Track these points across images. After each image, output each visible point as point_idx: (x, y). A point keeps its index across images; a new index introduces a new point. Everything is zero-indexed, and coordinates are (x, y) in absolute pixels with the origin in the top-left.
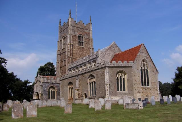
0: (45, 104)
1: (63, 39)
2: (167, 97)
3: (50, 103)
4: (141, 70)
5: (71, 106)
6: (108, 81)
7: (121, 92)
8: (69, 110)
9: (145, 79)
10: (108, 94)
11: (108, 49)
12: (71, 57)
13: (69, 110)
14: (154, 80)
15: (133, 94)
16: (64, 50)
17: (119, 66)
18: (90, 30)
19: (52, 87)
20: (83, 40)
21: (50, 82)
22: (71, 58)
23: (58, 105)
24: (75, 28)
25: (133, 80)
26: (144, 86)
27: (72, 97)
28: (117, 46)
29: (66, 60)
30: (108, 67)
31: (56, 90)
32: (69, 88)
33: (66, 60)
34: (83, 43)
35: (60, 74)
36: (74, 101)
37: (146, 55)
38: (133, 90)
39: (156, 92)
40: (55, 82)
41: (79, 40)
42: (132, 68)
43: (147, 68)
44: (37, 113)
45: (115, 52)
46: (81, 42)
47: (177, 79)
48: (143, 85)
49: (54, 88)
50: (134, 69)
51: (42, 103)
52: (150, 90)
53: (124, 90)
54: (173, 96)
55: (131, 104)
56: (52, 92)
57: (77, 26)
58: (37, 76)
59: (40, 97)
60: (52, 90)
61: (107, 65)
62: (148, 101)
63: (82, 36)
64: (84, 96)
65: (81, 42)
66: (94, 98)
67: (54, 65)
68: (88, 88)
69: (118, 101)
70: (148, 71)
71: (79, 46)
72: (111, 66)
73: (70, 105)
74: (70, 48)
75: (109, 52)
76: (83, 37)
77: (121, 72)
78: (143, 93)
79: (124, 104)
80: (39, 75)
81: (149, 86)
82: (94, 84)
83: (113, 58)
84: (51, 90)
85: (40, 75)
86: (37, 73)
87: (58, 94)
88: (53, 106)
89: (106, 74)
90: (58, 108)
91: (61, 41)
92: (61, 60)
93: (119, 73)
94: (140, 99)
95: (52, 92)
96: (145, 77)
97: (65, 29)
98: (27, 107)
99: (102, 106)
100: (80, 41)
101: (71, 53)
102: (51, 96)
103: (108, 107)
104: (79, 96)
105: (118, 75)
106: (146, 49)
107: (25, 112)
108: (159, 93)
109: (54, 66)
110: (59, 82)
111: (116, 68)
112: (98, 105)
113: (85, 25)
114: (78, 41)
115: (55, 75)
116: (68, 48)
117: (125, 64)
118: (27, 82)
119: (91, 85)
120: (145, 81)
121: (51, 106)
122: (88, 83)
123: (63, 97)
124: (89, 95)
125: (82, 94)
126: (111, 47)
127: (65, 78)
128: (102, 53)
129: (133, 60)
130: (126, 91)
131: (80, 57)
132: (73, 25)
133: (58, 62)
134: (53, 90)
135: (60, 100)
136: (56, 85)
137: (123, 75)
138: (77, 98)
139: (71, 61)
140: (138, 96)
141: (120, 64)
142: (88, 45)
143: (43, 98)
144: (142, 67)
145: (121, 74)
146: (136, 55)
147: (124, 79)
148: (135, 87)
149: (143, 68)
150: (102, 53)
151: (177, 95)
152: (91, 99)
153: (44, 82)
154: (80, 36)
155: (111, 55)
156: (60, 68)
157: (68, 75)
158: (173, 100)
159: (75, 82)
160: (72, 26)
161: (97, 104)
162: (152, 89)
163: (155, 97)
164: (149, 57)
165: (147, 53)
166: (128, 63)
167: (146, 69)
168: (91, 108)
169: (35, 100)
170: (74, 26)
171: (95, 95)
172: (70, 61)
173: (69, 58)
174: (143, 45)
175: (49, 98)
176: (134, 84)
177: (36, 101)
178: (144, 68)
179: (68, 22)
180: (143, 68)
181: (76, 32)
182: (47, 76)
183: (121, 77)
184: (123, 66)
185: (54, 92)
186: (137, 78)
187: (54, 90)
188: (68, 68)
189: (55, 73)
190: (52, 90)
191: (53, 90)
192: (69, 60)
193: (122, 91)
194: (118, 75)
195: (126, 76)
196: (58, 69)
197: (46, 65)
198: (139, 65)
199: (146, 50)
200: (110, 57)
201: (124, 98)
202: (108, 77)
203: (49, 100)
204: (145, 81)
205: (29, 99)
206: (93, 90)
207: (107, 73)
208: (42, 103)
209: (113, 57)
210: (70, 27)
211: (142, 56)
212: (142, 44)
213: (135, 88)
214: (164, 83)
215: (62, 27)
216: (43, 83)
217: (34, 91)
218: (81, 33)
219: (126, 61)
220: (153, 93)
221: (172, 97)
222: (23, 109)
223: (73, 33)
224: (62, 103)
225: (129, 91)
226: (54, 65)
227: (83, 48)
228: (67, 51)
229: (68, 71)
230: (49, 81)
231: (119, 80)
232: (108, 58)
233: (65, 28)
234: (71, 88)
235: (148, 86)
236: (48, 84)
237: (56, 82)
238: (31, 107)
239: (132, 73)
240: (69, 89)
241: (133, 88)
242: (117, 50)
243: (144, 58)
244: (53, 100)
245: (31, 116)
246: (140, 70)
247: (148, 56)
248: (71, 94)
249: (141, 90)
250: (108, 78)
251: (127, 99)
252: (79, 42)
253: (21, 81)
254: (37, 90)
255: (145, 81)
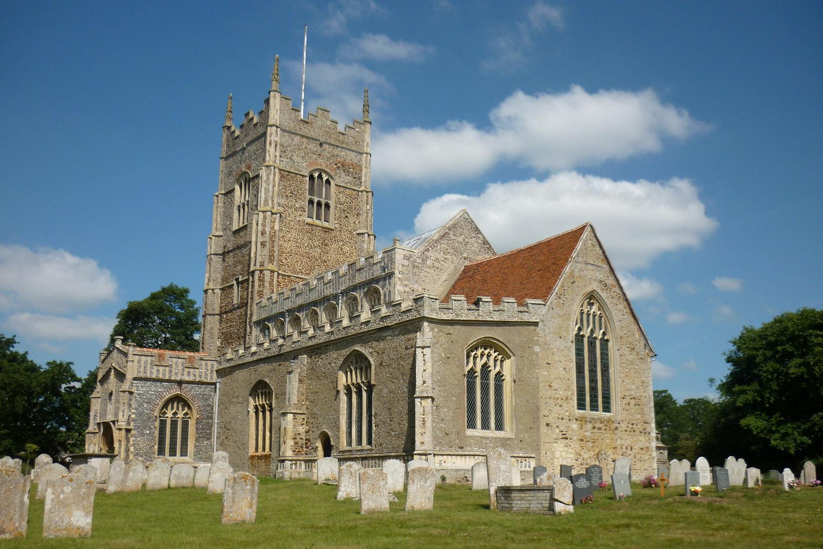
0: (140, 475)
1: (237, 187)
2: (686, 463)
3: (162, 473)
4: (579, 338)
5: (252, 491)
6: (429, 382)
7: (486, 433)
8: (242, 506)
9: (593, 380)
10: (423, 439)
11: (437, 241)
12: (270, 267)
13: (242, 506)
14: (633, 387)
15: (537, 449)
16: (242, 234)
17: (480, 319)
18: (363, 154)
19: (177, 399)
20: (328, 196)
21: (154, 376)
22: (272, 272)
23: (197, 482)
24: (297, 139)
25: (541, 385)
26: (588, 413)
27: (264, 449)
28: (477, 230)
29: (247, 280)
30: (431, 321)
31: (195, 415)
32: (256, 407)
33: (247, 280)
34: (327, 206)
35: (218, 344)
36: (273, 467)
37: (600, 276)
38: (538, 427)
39: (642, 441)
40: (191, 378)
41: (311, 192)
42: (538, 329)
43: (604, 334)
44: (93, 518)
45: (465, 255)
46: (319, 204)
47: (737, 388)
48: (585, 409)
49: (186, 404)
50: (545, 332)
51: (126, 473)
52: (616, 428)
53: (499, 426)
54: (717, 461)
55: (521, 490)
56: (174, 423)
57: (305, 130)
58: (113, 341)
59: (116, 445)
60: (175, 414)
61: (427, 313)
62: (601, 478)
63: (325, 178)
64: (319, 445)
65: (319, 204)
66: (363, 459)
67: (190, 297)
68: (337, 411)
69: (469, 475)
70: (610, 344)
71: (309, 220)
72: (445, 317)
73: (249, 487)
74: (267, 230)
75: (441, 256)
76: (328, 182)
77: (486, 344)
78: (582, 440)
79: (492, 491)
80: (118, 344)
81: (609, 412)
82: (364, 394)
83: (458, 280)
84: (169, 414)
85: (124, 342)
86: (110, 331)
87: (204, 433)
88: (176, 488)
89: (419, 351)
90: (196, 495)
91: (230, 192)
92: (224, 279)
93: (476, 349)
94: (565, 471)
95: (174, 423)
96: (593, 371)
97: (249, 144)
98: (50, 491)
99: (397, 494)
100: (316, 200)
101: (272, 251)
102: (169, 441)
103: (421, 498)
104: (296, 443)
105: (475, 358)
106: (601, 247)
107: (37, 505)
108: (654, 444)
109: (193, 303)
110: (209, 380)
111: (464, 328)
112: (374, 489)
113: (341, 128)
114: (308, 197)
115: (193, 346)
116: (260, 228)
117: (509, 309)
118: (62, 371)
119: (354, 396)
120: (594, 390)
121: (166, 489)
122: (341, 388)
123: (225, 450)
124: (344, 445)
125: (312, 436)
126: (451, 233)
127: (240, 362)
128: (407, 258)
129: (543, 293)
130: (508, 432)
131: (312, 269)
132: (291, 126)
133: (211, 286)
134: (180, 415)
135: (209, 459)
136: (198, 390)
137: (495, 361)
138: (289, 454)
139: (271, 283)
140: (557, 454)
141: (488, 310)
142: (352, 219)
143: (132, 449)
144: (580, 329)
145: (489, 356)
146: (556, 274)
147: (499, 376)
148: (546, 413)
149: (586, 332)
150: (407, 258)
151: (731, 460)
152: (348, 463)
153: (142, 375)
154: (316, 175)
155: (451, 268)
156: (220, 315)
157: (254, 349)
158: (715, 478)
159: (283, 383)
160: (284, 131)
161: (376, 487)
162: (623, 426)
163: (634, 456)
164: (615, 283)
165: (605, 266)
166: (520, 305)
167: (599, 334)
168: (348, 501)
169: (93, 460)
170: (289, 132)
171: (370, 442)
172: (267, 284)
173: (261, 271)
174: (588, 229)
175: (161, 452)
176: (542, 403)
177: (94, 462)
178: (592, 331)
179: (264, 114)
180: (586, 332)
181: (300, 160)
182: (156, 351)
183: (485, 367)
184: (496, 317)
185: (185, 424)
186: (559, 372)
187: (186, 414)
188: (255, 319)
189: (197, 336)
190: (175, 414)
191: (180, 415)
192: (261, 280)
193: (175, 455)
194: (475, 358)
195: (507, 363)
196: (209, 318)
197: (154, 297)
198: (568, 319)
199: (604, 252)
200: (445, 276)
201: (492, 463)
202: (429, 364)
203: (159, 460)
204: (594, 390)
205: (67, 450)
206: (366, 416)
207: (423, 348)
208: (126, 473)
209: (456, 278)
210: (273, 135)
211: (580, 273)
212: (585, 227)
213: (550, 419)
214: (685, 401)
215: (237, 133)
216: (135, 379)
217: (92, 414)
218: (322, 164)
219: (512, 300)
220: (627, 443)
221: (712, 464)
222: (26, 499)
223: (285, 160)
224: (216, 473)
225: (518, 431)
226: (190, 297)
227: (327, 230)
228: (254, 239)
229: (256, 331)
230: (163, 373)
231: (478, 381)
232: (435, 283)
233: (249, 139)
234: (263, 407)
235: (604, 411)
236: (159, 384)
237: (198, 379)
238: (68, 489)
239: (537, 354)
240: (252, 410)
241: (536, 419)
242: (475, 245)
243: (595, 286)
244: (178, 458)
245: (64, 532)
246: (572, 336)
247: (611, 281)
248: (261, 433)
249: (573, 430)
250: (429, 371)
251: (503, 467)
252: (311, 202)
253: (34, 368)
254: (104, 412)
255: (593, 389)
